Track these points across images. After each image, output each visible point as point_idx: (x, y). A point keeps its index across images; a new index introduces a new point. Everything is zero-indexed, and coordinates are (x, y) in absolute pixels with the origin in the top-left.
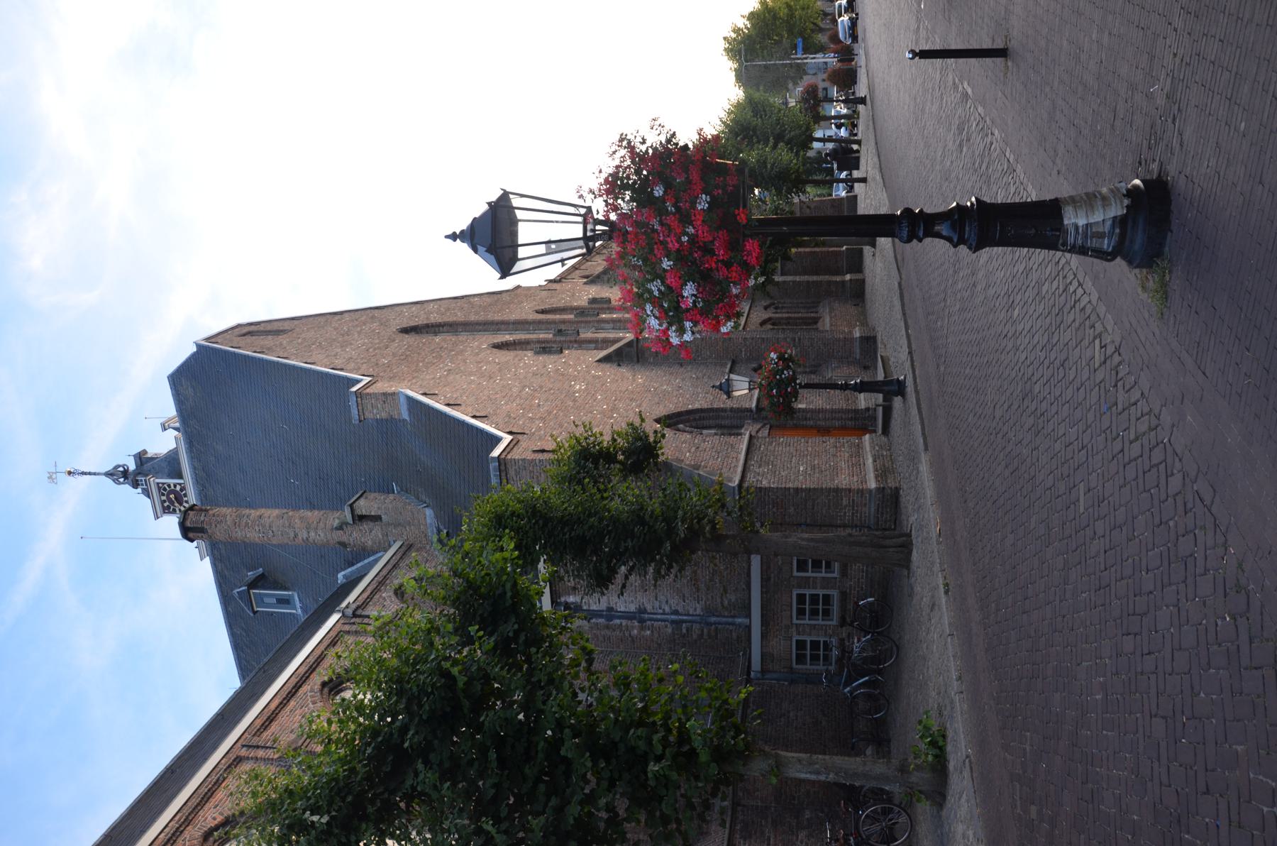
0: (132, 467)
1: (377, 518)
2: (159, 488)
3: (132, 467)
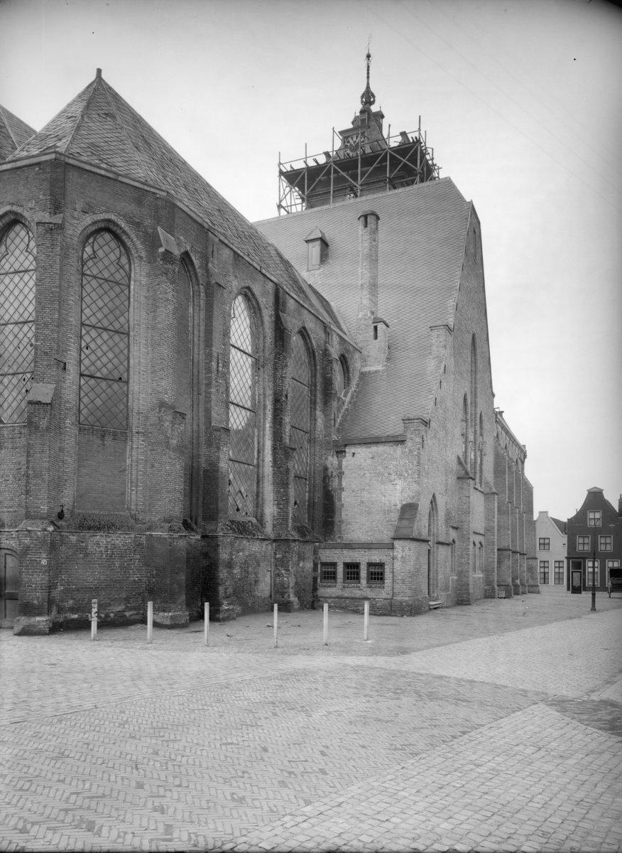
0: (374, 108)
1: (376, 337)
3: (374, 108)
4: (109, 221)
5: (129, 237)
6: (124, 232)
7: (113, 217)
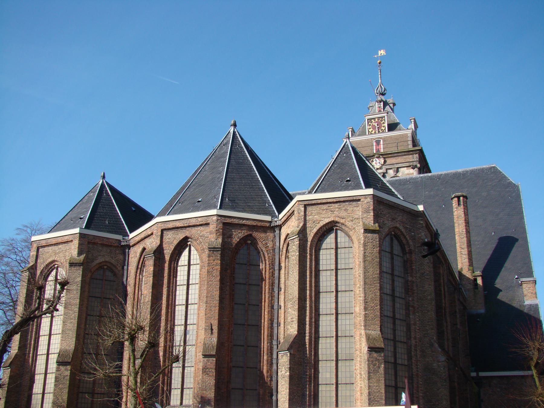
2: (382, 117)
4: (396, 227)
5: (405, 237)
6: (404, 235)
7: (398, 225)
